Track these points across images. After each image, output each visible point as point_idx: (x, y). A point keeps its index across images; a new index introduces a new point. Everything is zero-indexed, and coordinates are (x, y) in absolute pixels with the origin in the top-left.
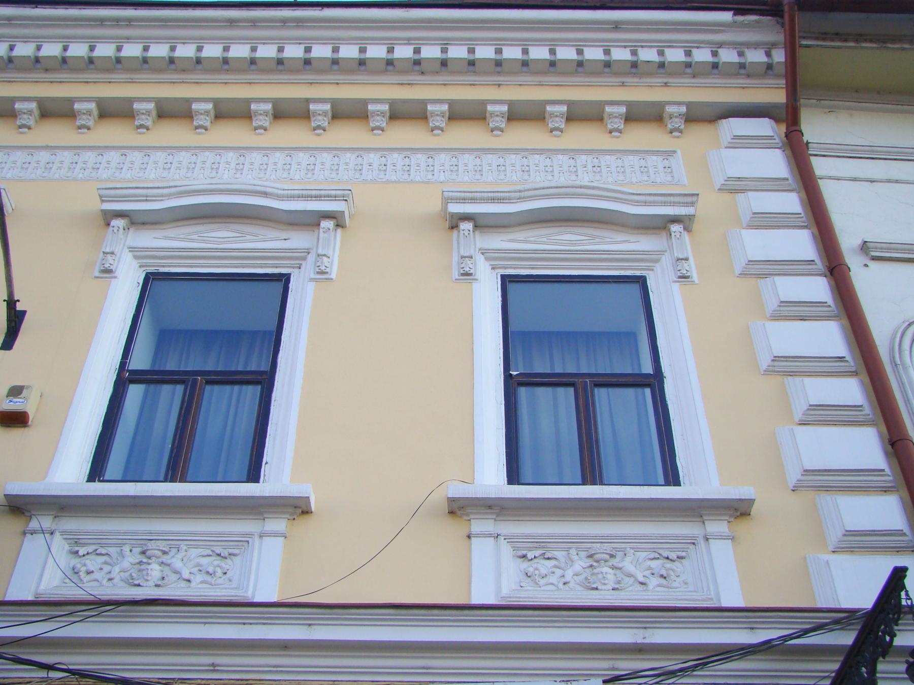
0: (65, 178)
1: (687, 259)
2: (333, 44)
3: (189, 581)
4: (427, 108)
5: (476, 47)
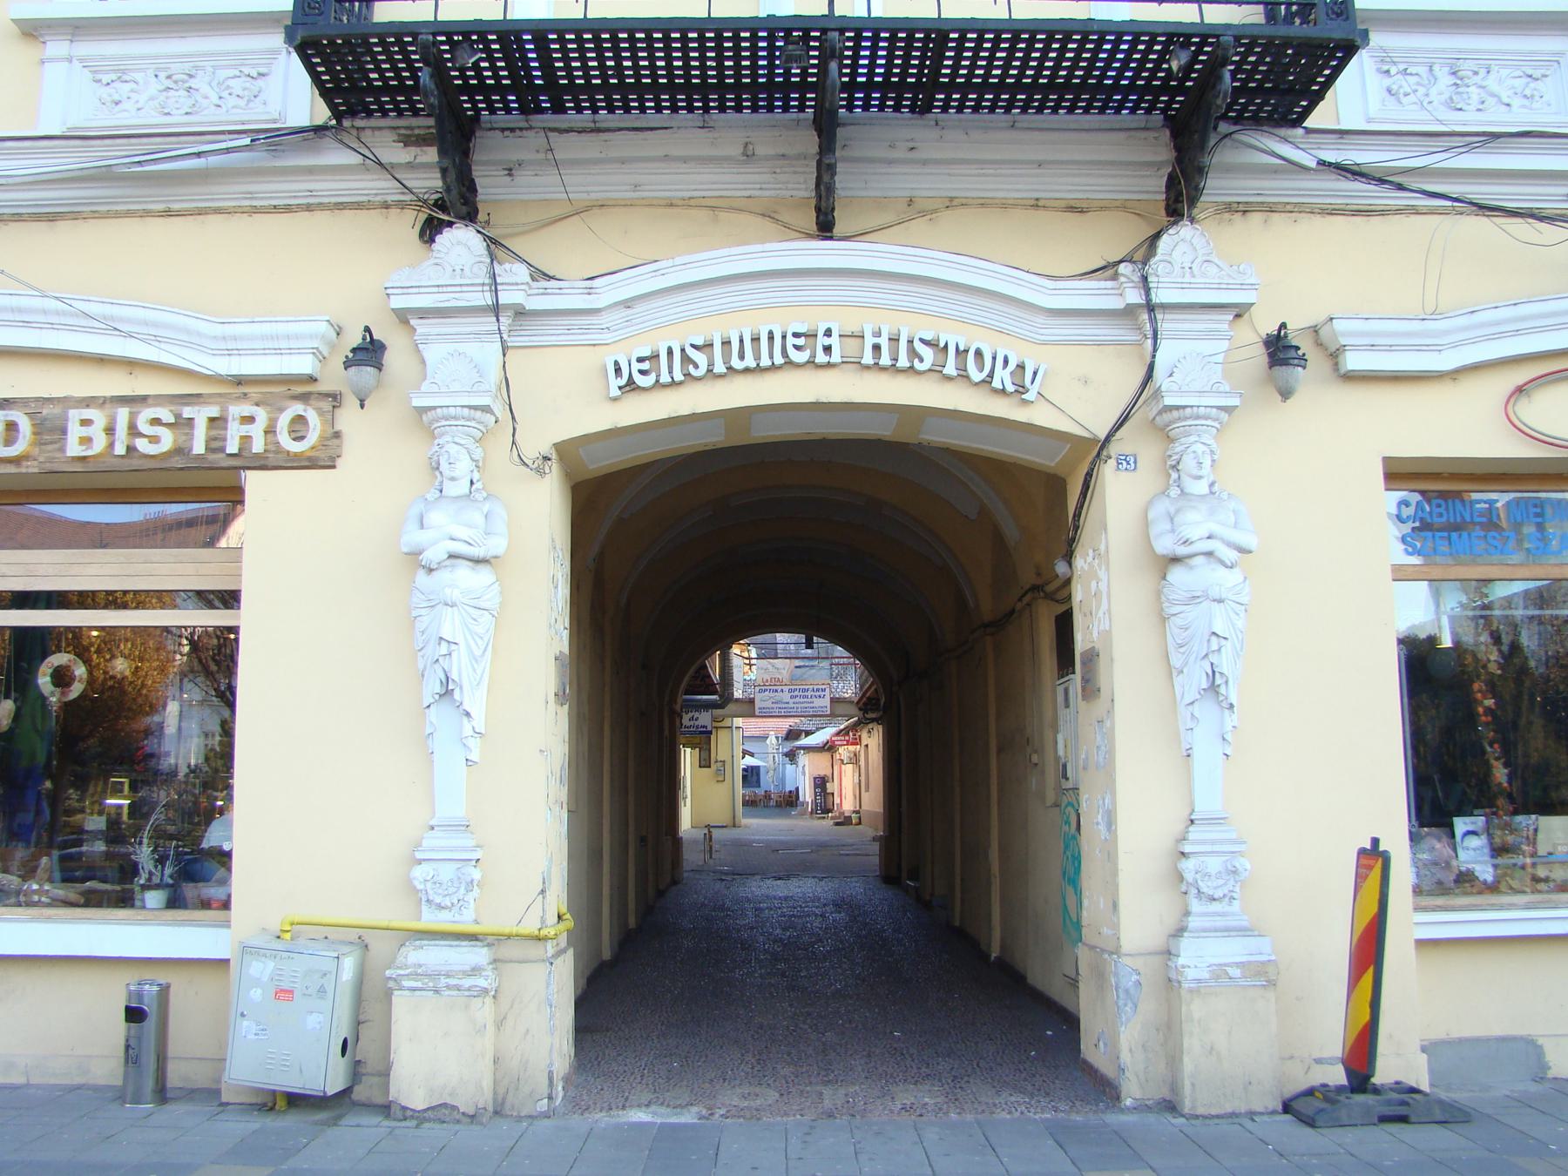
3: (1508, 105)
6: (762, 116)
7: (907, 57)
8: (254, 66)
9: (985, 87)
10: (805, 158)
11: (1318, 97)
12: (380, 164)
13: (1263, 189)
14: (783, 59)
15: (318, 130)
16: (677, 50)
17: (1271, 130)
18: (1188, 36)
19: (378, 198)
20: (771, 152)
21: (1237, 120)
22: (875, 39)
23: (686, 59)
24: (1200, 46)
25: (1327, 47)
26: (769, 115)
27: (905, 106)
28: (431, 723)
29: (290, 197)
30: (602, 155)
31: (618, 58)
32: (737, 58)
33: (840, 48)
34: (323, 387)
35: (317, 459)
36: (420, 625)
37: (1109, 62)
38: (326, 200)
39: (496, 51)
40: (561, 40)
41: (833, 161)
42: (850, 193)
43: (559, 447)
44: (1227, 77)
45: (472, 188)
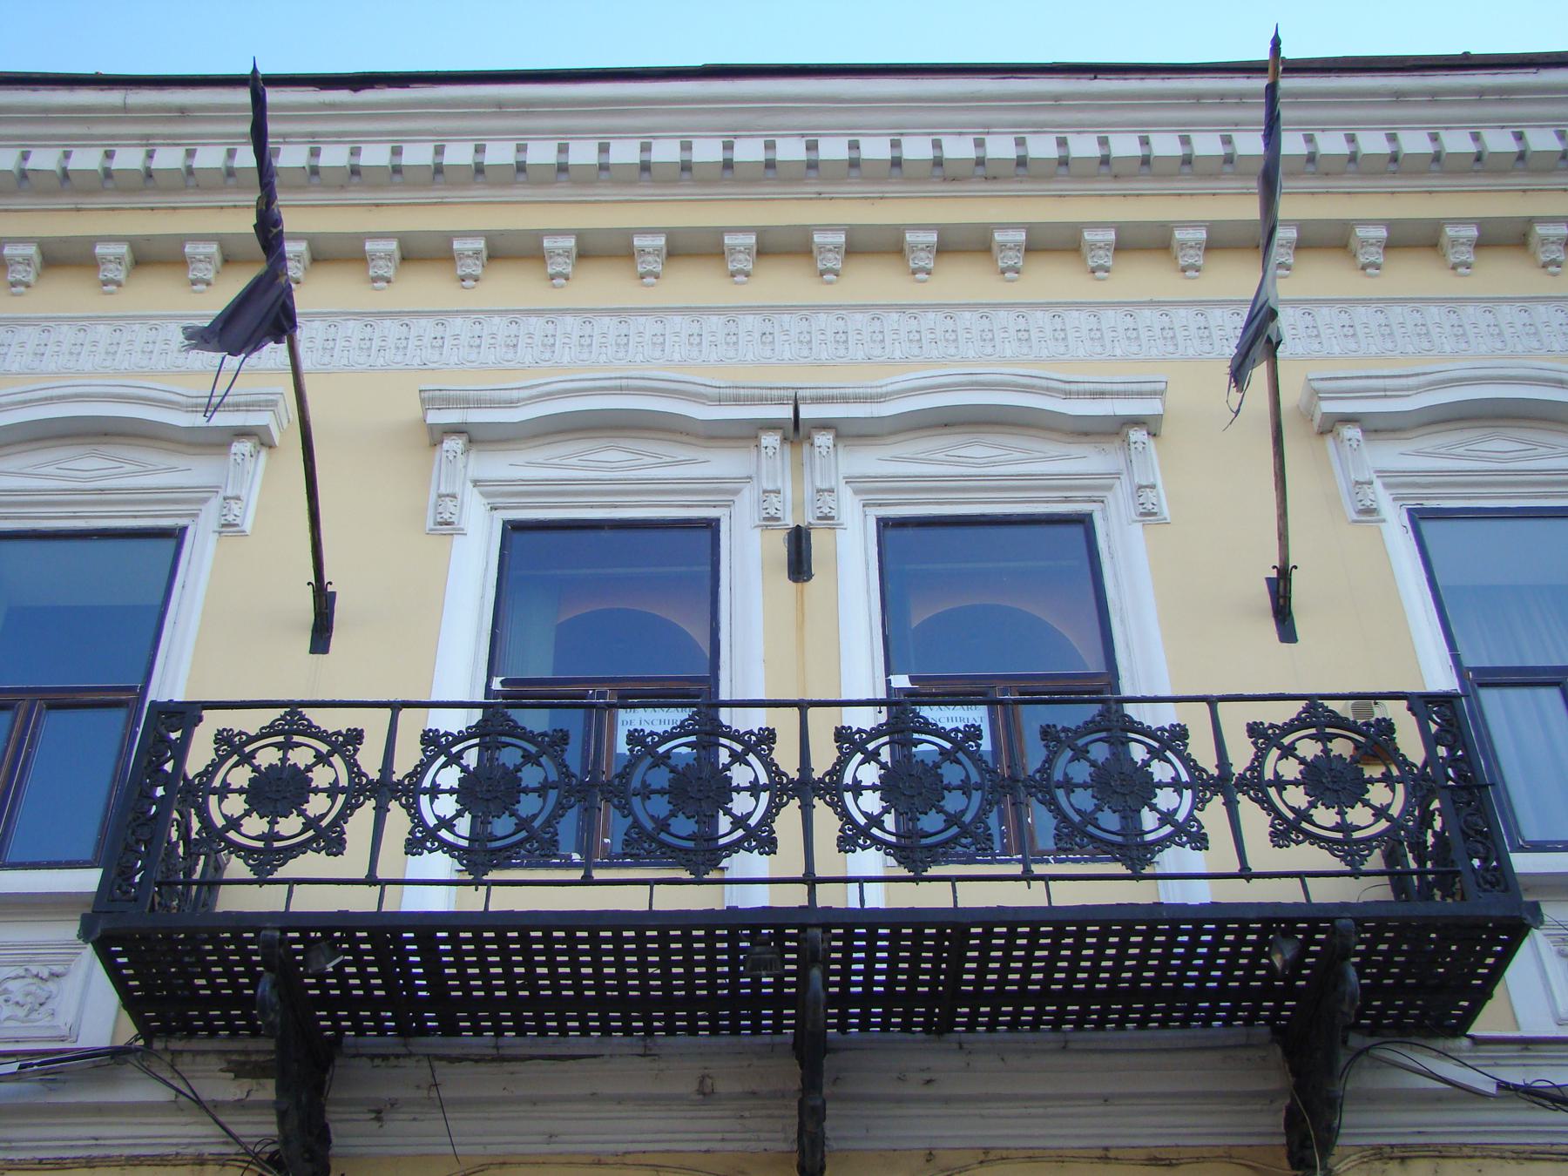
0: (174, 369)
1: (1153, 487)
2: (1017, 133)
4: (812, 238)
5: (693, 140)
6: (725, 1039)
7: (915, 960)
8: (45, 964)
9: (1023, 996)
10: (783, 1096)
11: (1482, 995)
12: (198, 1101)
13: (1427, 1125)
14: (748, 965)
15: (116, 1054)
16: (608, 953)
17: (1423, 1042)
18: (1291, 922)
19: (191, 1150)
20: (737, 1088)
21: (1372, 1031)
22: (872, 937)
23: (620, 965)
24: (1309, 934)
25: (1485, 929)
26: (734, 1039)
27: (918, 1024)
29: (65, 1147)
30: (506, 1093)
31: (530, 964)
32: (689, 964)
33: (824, 950)
37: (1187, 958)
38: (116, 1152)
39: (367, 952)
40: (454, 939)
41: (819, 1102)
42: (843, 1145)
44: (1352, 973)
45: (324, 1137)
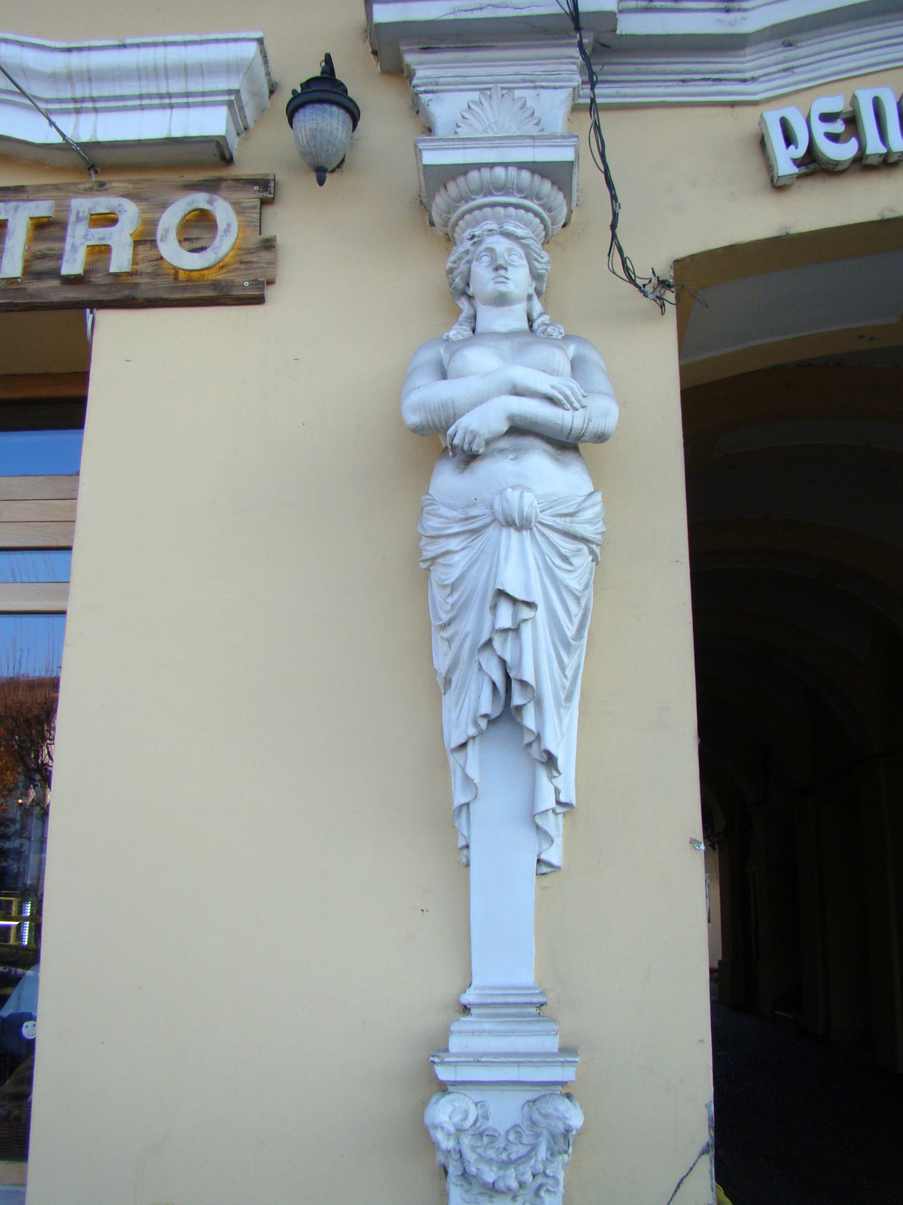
28: (467, 779)
34: (244, 168)
35: (230, 285)
36: (443, 574)
43: (680, 265)
